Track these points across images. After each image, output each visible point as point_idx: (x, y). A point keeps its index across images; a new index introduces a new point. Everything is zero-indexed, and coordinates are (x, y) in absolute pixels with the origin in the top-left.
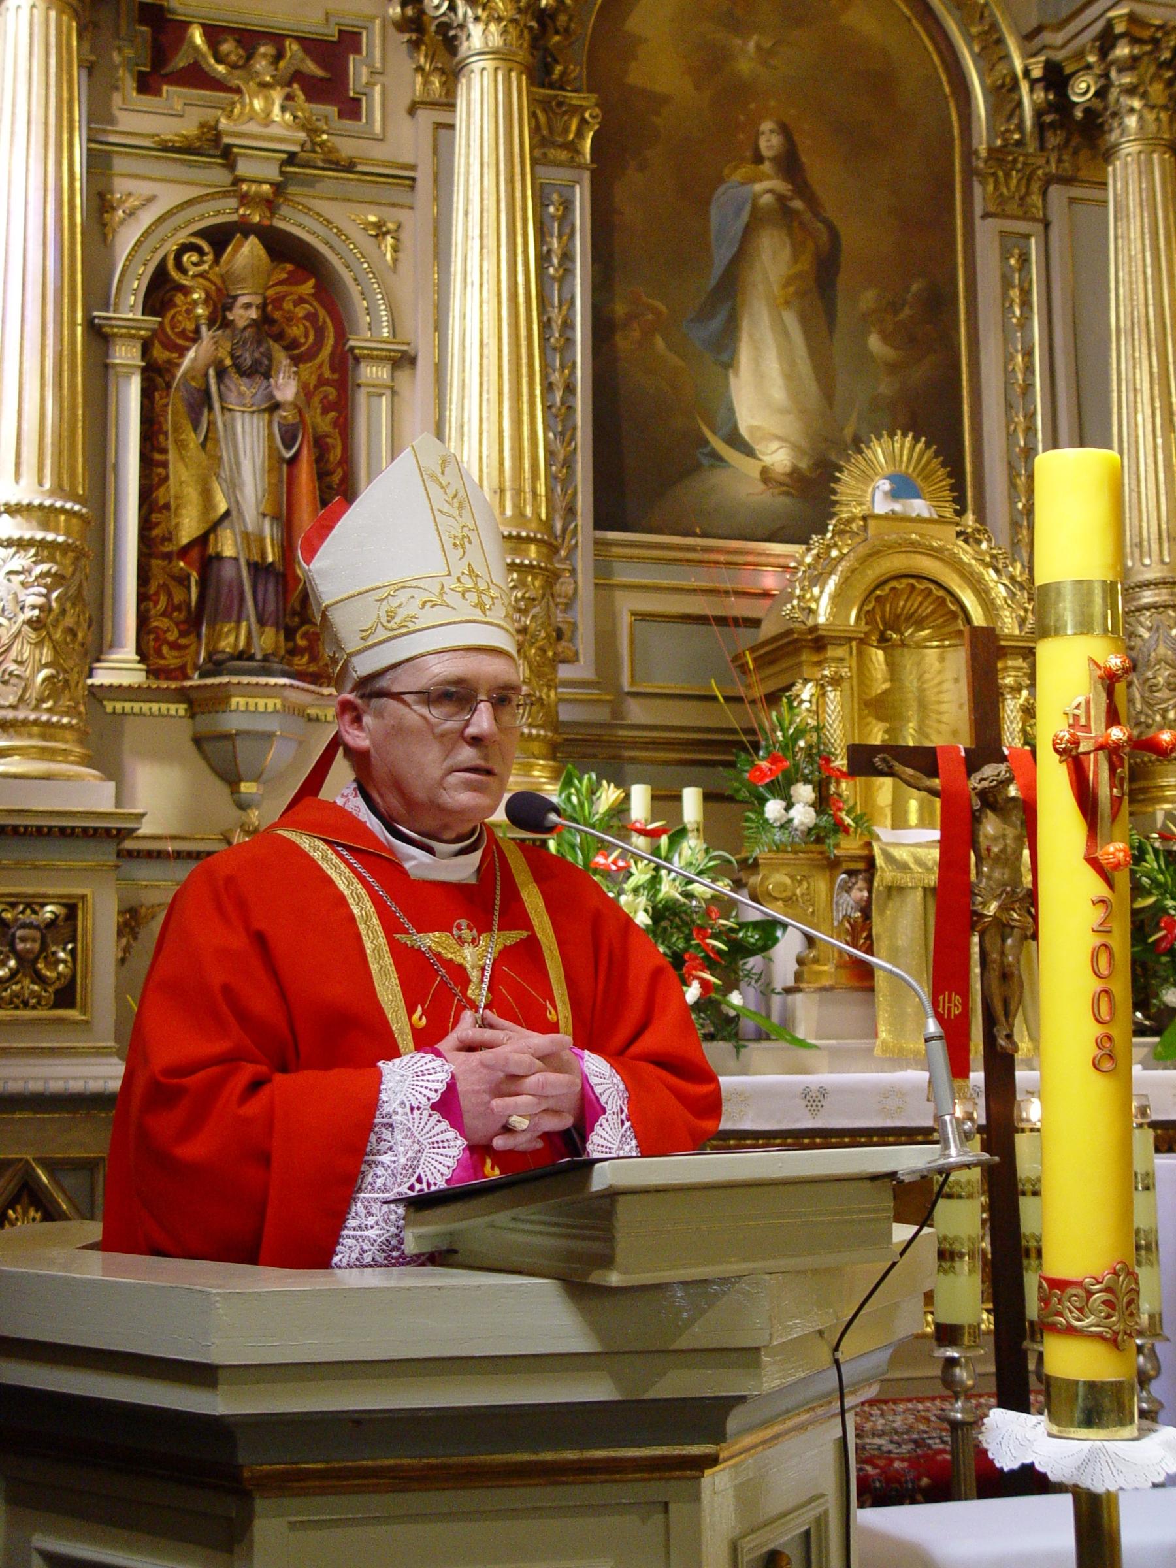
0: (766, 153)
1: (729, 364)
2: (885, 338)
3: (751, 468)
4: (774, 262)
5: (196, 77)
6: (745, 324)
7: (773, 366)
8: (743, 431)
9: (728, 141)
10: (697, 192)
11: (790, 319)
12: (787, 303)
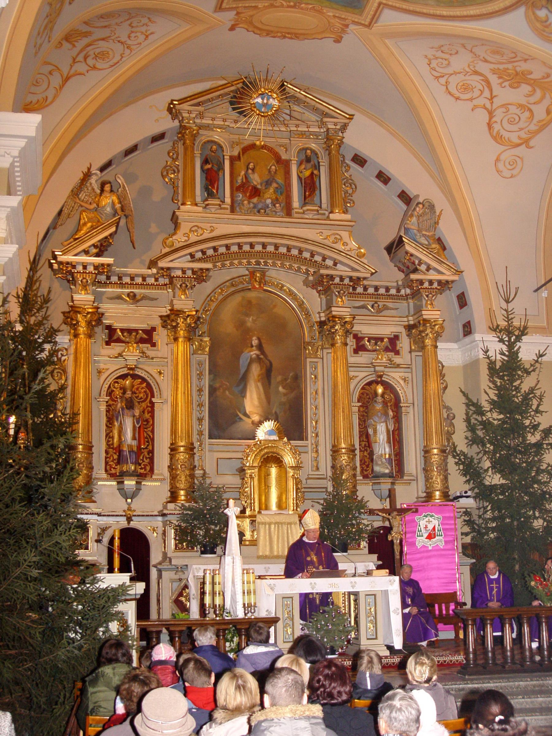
0: (254, 344)
1: (244, 396)
2: (284, 388)
3: (249, 421)
4: (256, 370)
5: (119, 340)
6: (248, 387)
7: (255, 396)
8: (247, 412)
9: (245, 342)
10: (237, 356)
11: (259, 384)
12: (259, 381)
